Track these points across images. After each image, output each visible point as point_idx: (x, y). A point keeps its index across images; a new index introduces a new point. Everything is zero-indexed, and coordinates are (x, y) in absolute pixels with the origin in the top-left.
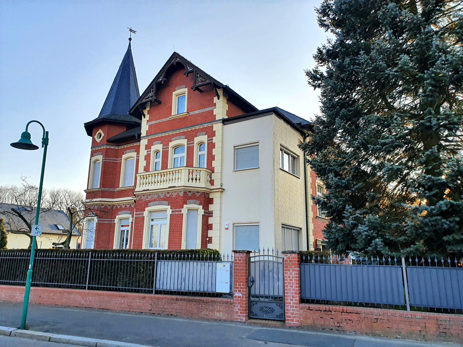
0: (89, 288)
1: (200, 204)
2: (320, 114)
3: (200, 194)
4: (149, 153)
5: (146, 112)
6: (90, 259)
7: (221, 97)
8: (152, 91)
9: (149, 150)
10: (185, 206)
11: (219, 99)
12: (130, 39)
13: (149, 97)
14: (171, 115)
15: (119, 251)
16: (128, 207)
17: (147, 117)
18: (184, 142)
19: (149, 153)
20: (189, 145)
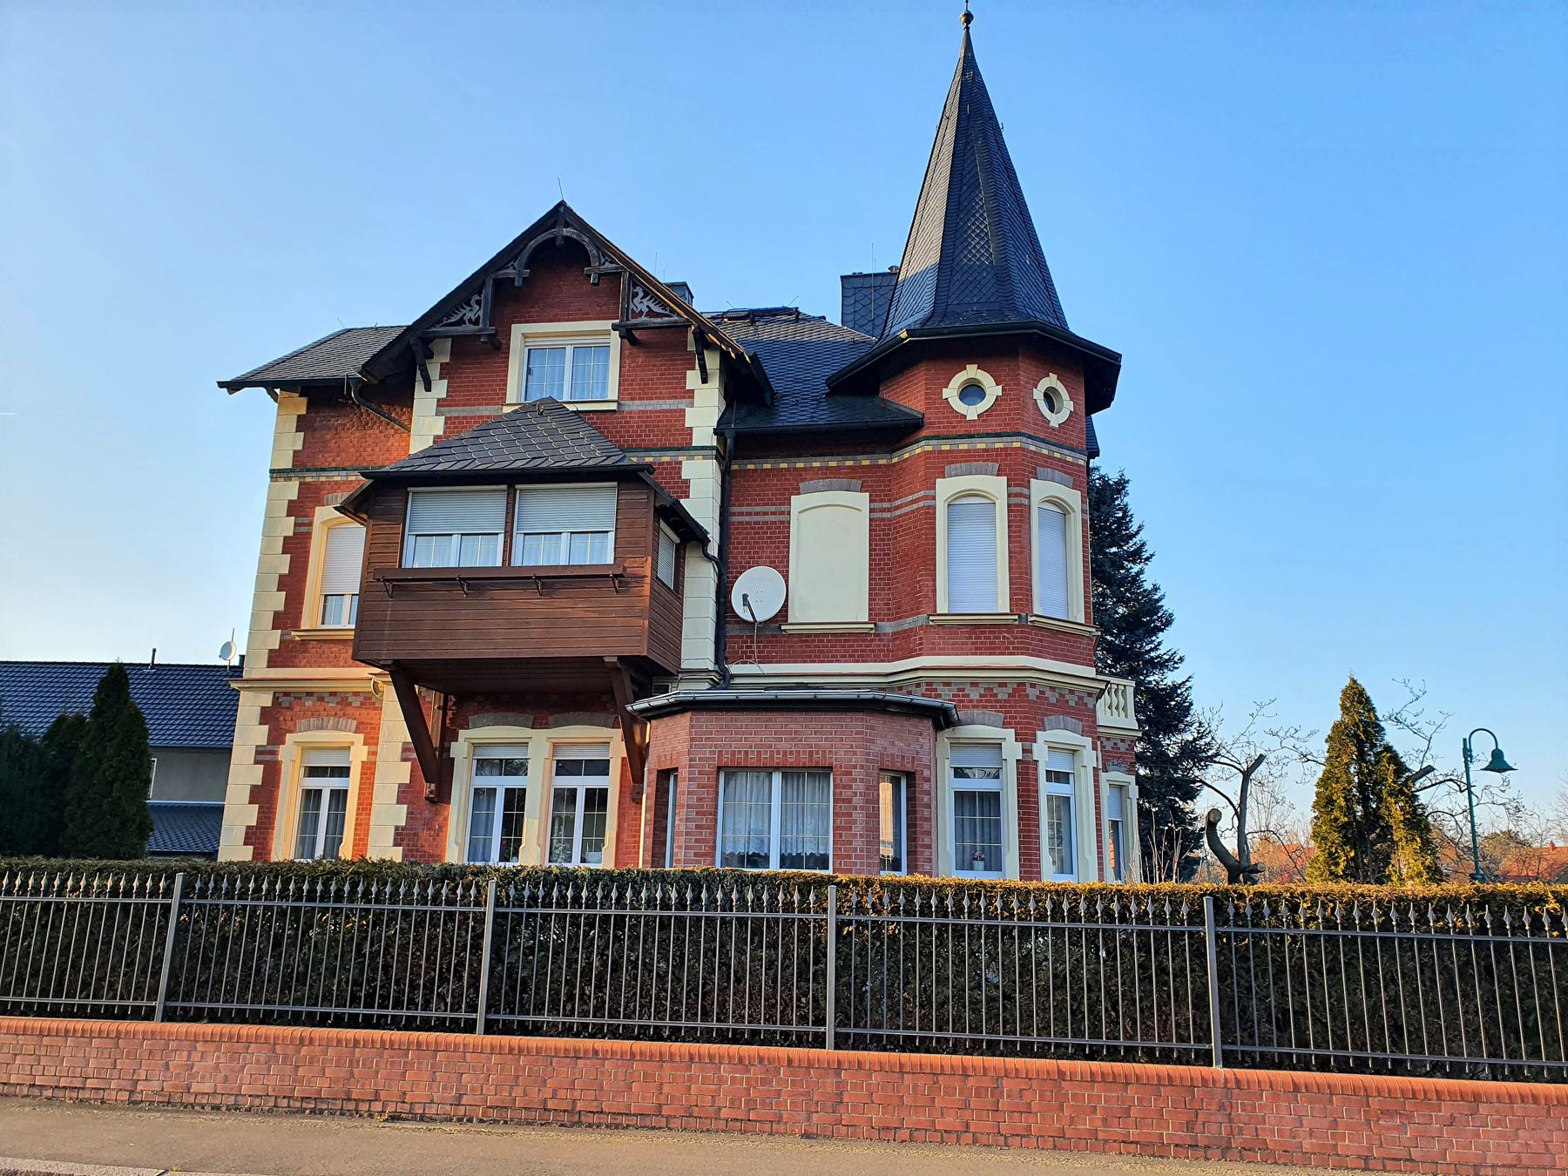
0: (490, 1028)
1: (1005, 725)
2: (1126, 500)
3: (361, 699)
4: (303, 529)
5: (434, 370)
6: (489, 910)
7: (715, 383)
8: (478, 302)
9: (306, 520)
10: (462, 734)
11: (705, 381)
12: (969, 18)
13: (461, 322)
14: (502, 401)
15: (549, 879)
16: (1053, 700)
17: (441, 388)
18: (996, 486)
19: (303, 529)
20: (876, 515)
